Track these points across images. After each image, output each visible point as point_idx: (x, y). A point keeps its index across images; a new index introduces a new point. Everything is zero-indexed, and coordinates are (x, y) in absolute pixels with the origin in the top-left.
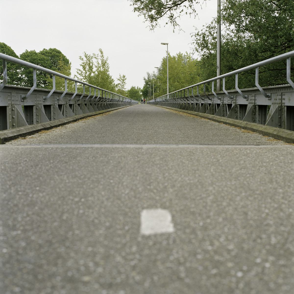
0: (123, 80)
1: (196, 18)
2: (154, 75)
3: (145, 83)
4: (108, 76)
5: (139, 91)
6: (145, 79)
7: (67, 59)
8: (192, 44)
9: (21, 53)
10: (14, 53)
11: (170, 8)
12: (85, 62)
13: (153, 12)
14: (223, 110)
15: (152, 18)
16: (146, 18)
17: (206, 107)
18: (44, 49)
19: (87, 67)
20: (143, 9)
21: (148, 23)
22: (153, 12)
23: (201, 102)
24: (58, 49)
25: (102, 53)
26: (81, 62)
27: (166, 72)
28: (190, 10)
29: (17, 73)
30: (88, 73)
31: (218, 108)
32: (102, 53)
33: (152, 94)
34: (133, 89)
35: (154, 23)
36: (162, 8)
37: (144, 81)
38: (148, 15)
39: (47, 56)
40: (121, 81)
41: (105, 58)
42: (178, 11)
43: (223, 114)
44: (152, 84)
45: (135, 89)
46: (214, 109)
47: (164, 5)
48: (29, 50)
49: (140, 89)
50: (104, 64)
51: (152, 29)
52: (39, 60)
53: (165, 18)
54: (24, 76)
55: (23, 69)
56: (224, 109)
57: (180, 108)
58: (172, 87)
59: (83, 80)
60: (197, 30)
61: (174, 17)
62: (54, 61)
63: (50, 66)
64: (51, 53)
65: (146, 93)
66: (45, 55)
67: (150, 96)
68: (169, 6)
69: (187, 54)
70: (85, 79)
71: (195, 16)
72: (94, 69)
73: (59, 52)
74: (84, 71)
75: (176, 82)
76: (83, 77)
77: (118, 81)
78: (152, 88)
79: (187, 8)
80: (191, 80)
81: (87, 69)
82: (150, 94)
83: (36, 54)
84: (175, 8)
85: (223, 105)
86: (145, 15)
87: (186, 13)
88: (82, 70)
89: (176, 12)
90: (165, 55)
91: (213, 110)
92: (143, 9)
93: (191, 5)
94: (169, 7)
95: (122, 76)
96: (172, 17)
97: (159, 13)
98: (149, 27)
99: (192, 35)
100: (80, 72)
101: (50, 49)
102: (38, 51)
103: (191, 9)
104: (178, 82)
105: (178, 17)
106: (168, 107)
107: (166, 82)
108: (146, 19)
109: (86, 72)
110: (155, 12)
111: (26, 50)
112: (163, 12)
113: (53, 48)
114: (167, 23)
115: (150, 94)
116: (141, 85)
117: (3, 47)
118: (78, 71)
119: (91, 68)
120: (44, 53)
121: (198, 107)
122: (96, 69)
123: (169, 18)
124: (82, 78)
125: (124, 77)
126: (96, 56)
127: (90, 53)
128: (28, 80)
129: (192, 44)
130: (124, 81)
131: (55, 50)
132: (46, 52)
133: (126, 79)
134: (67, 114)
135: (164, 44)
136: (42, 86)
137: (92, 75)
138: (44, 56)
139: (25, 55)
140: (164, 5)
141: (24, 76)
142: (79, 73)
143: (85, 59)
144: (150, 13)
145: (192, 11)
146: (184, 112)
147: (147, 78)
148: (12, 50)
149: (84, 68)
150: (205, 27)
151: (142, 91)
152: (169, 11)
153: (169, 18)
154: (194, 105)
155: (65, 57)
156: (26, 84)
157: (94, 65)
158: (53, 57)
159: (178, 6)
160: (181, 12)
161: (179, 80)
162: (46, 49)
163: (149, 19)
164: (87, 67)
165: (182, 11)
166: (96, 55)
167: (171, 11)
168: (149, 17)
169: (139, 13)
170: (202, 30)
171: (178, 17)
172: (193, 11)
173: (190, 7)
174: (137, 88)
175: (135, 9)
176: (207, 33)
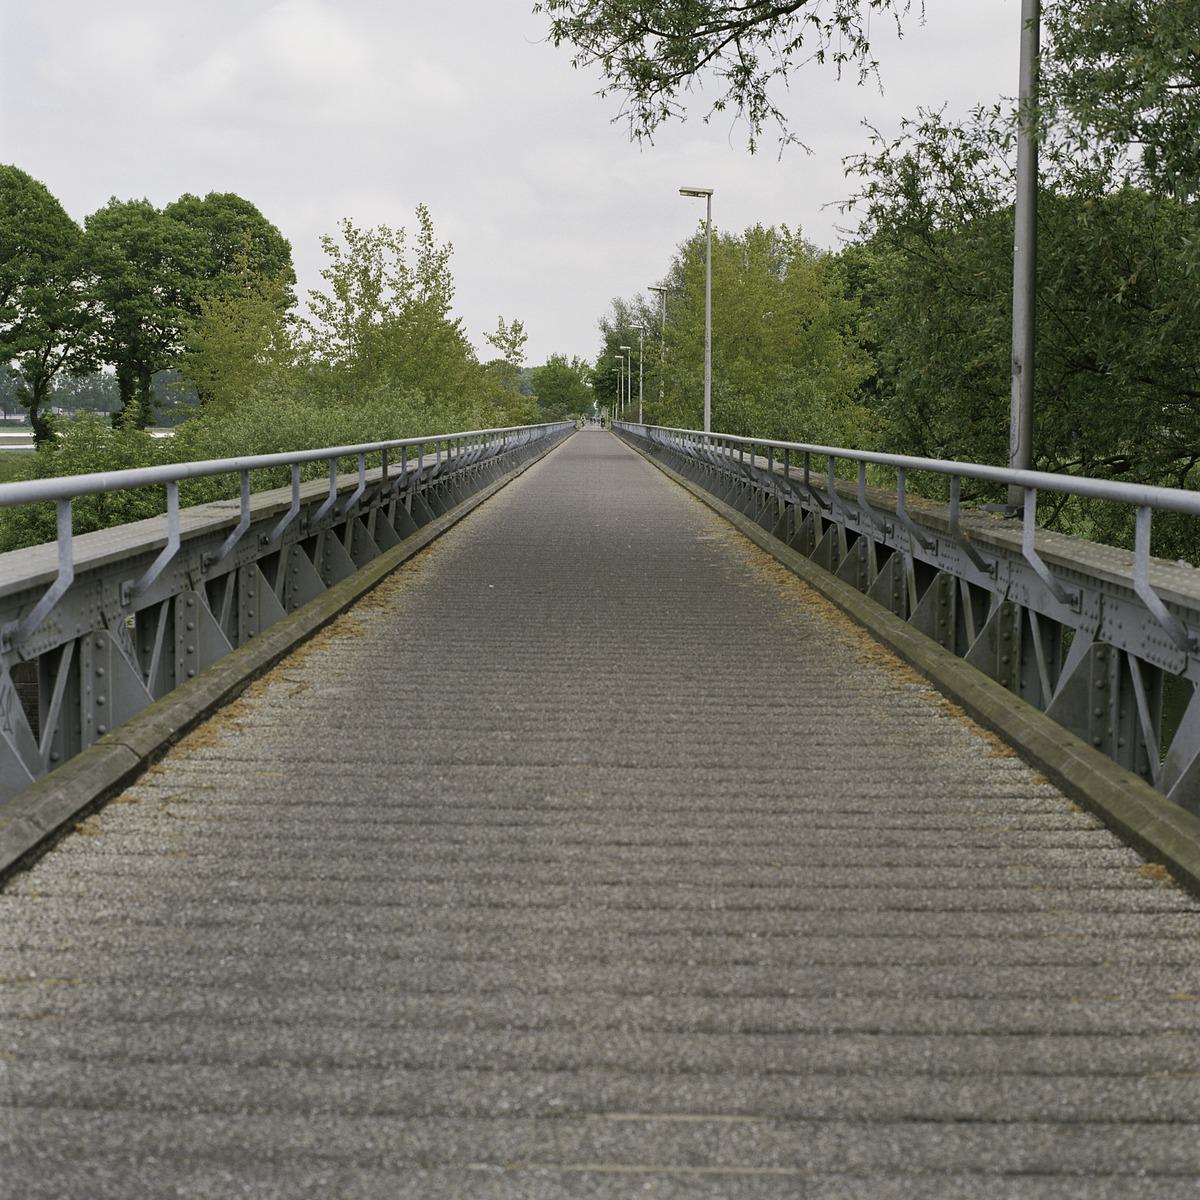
0: (513, 344)
1: (867, 81)
2: (644, 312)
3: (605, 345)
4: (451, 336)
5: (579, 377)
6: (605, 328)
7: (281, 241)
8: (842, 208)
9: (92, 212)
10: (60, 211)
11: (739, 29)
12: (347, 262)
13: (651, 45)
14: (1099, 683)
15: (644, 75)
16: (615, 71)
17: (952, 593)
18: (187, 197)
19: (355, 288)
20: (598, 27)
21: (623, 98)
22: (651, 45)
23: (912, 551)
24: (244, 195)
25: (427, 226)
26: (328, 261)
27: (696, 308)
28: (840, 42)
29: (75, 297)
30: (358, 312)
31: (850, 545)
32: (427, 226)
33: (635, 394)
34: (556, 364)
35: (658, 98)
36: (702, 29)
37: (602, 335)
38: (626, 61)
39: (196, 226)
40: (502, 347)
41: (438, 247)
42: (779, 41)
43: (1097, 711)
44: (636, 349)
45: (565, 367)
46: (1017, 634)
47: (711, 14)
48: (125, 201)
49: (585, 366)
50: (433, 272)
51: (643, 130)
52: (165, 240)
53: (711, 78)
54: (99, 308)
55: (95, 280)
56: (1105, 676)
57: (780, 535)
58: (723, 377)
59: (337, 340)
60: (879, 142)
61: (757, 74)
62: (227, 249)
63: (210, 269)
64: (214, 214)
65: (609, 385)
66: (187, 222)
67: (626, 398)
68: (733, 16)
69: (787, 233)
70: (343, 338)
71: (864, 72)
72: (386, 295)
73: (248, 210)
74: (341, 304)
75: (742, 358)
76: (335, 326)
77: (492, 345)
78: (635, 367)
79: (824, 31)
80: (805, 348)
81: (352, 294)
82: (626, 388)
83: (148, 214)
84: (763, 26)
85: (1099, 654)
86: (607, 59)
87: (821, 54)
88: (332, 296)
89: (764, 51)
90: (691, 231)
91: (1008, 639)
92: (598, 27)
93: (844, 14)
94: (731, 25)
95: (509, 324)
96: (746, 71)
97: (685, 55)
98: (624, 121)
99: (850, 163)
100: (322, 307)
101: (212, 197)
102: (160, 204)
103: (846, 38)
104: (749, 356)
105: (777, 71)
106: (709, 497)
107: (696, 358)
108: (612, 80)
109: (347, 304)
110: (662, 43)
111: (113, 198)
112: (702, 44)
113: (222, 190)
114: (720, 106)
115: (626, 388)
116: (587, 350)
117: (12, 186)
118: (317, 302)
119: (371, 289)
120: (186, 210)
121: (895, 574)
122: (394, 294)
123: (730, 75)
124: (333, 331)
125: (517, 328)
126: (394, 236)
127: (366, 225)
128: (118, 325)
129: (842, 208)
130: (517, 349)
131: (232, 202)
132: (193, 210)
133: (524, 339)
134: (105, 692)
135: (695, 194)
136: (173, 352)
137: (377, 318)
138: (182, 225)
139: (104, 221)
140: (711, 14)
141: (99, 308)
142: (318, 310)
143: (346, 249)
144: (634, 51)
145: (848, 47)
146: (811, 586)
147: (612, 323)
148: (50, 197)
149: (342, 291)
150: (911, 129)
151: (592, 375)
152: (733, 43)
153: (730, 75)
154: (865, 546)
155: (273, 229)
156: (106, 340)
157: (384, 279)
158: (221, 228)
159: (782, 17)
160: (789, 50)
161: (752, 349)
162: (194, 194)
163: (625, 79)
164: (355, 286)
165: (795, 43)
166: (393, 233)
167: (744, 41)
168: (628, 69)
169: (579, 50)
170: (898, 144)
171: (777, 71)
172: (853, 44)
173: (839, 26)
174: (575, 362)
175: (559, 30)
176: (925, 162)
